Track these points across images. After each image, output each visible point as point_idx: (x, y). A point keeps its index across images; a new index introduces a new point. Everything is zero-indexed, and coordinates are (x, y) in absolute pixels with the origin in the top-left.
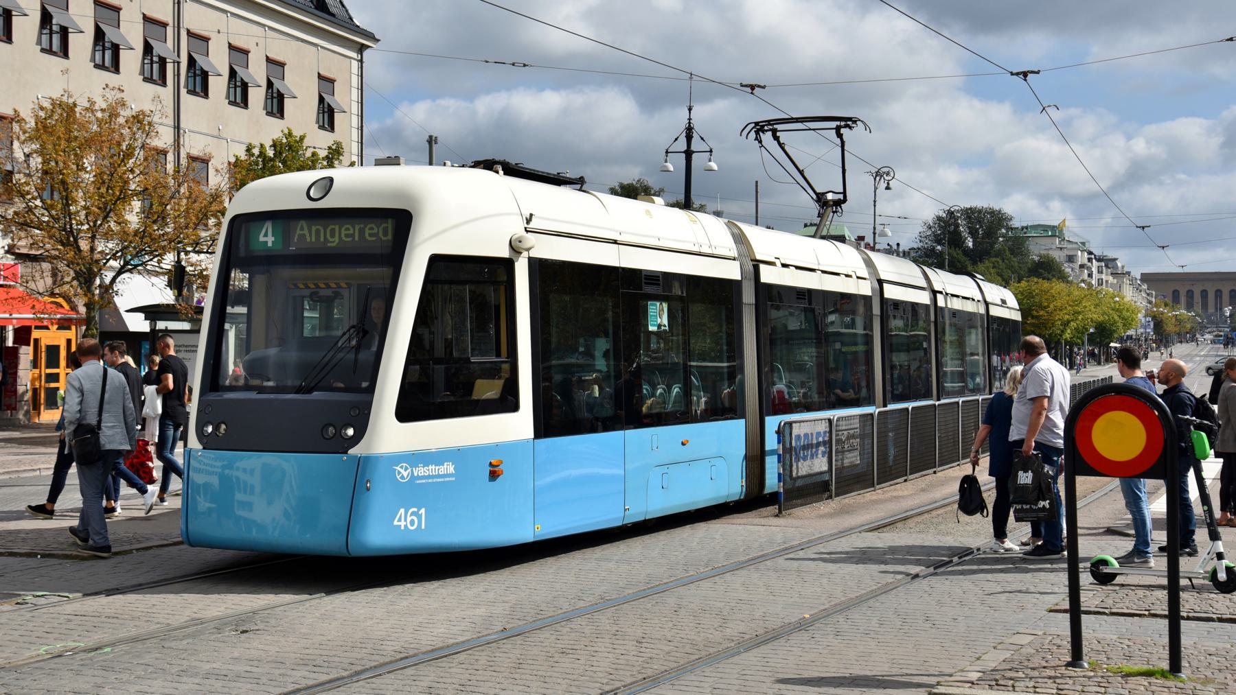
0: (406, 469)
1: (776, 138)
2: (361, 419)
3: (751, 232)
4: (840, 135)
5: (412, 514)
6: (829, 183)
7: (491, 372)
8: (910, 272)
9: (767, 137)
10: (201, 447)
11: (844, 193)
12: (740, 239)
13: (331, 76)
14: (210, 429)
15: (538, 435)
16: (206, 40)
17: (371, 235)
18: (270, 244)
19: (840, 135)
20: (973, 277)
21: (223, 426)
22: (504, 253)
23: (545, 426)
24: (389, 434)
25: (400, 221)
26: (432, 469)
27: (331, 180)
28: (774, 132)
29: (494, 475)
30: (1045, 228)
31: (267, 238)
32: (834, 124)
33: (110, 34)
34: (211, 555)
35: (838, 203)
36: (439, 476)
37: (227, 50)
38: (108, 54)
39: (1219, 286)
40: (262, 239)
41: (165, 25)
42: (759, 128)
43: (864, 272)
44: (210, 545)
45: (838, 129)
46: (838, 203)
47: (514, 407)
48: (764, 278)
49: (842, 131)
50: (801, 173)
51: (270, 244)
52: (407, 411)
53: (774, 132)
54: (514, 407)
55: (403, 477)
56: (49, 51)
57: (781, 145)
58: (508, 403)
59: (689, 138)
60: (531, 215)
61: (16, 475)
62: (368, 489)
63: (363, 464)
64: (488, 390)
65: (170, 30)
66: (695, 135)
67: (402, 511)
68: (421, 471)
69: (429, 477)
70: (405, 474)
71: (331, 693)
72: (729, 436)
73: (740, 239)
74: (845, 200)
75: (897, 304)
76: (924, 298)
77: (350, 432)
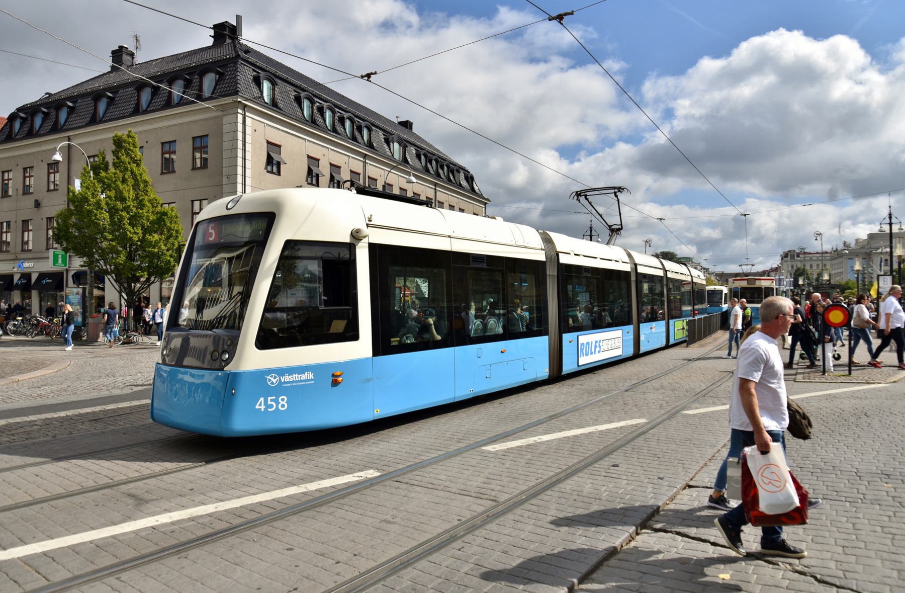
0: (275, 377)
1: (587, 199)
2: (231, 346)
3: (555, 236)
4: (616, 196)
6: (614, 221)
7: (338, 316)
8: (655, 262)
9: (582, 199)
12: (548, 241)
13: (317, 157)
15: (376, 353)
16: (280, 146)
19: (616, 196)
20: (685, 265)
22: (347, 239)
23: (382, 346)
24: (251, 358)
25: (266, 219)
26: (296, 377)
29: (335, 383)
30: (687, 258)
32: (613, 191)
33: (315, 170)
34: (173, 433)
35: (619, 230)
36: (301, 381)
38: (314, 179)
41: (359, 174)
42: (578, 194)
43: (627, 259)
44: (166, 425)
45: (615, 193)
46: (619, 230)
47: (355, 337)
48: (561, 261)
52: (265, 341)
53: (586, 196)
54: (355, 337)
55: (272, 383)
56: (272, 172)
57: (590, 203)
58: (351, 334)
62: (233, 394)
63: (235, 376)
64: (338, 326)
65: (361, 176)
68: (287, 378)
69: (293, 382)
70: (274, 381)
71: (85, 588)
72: (540, 345)
73: (548, 241)
75: (645, 276)
76: (660, 273)
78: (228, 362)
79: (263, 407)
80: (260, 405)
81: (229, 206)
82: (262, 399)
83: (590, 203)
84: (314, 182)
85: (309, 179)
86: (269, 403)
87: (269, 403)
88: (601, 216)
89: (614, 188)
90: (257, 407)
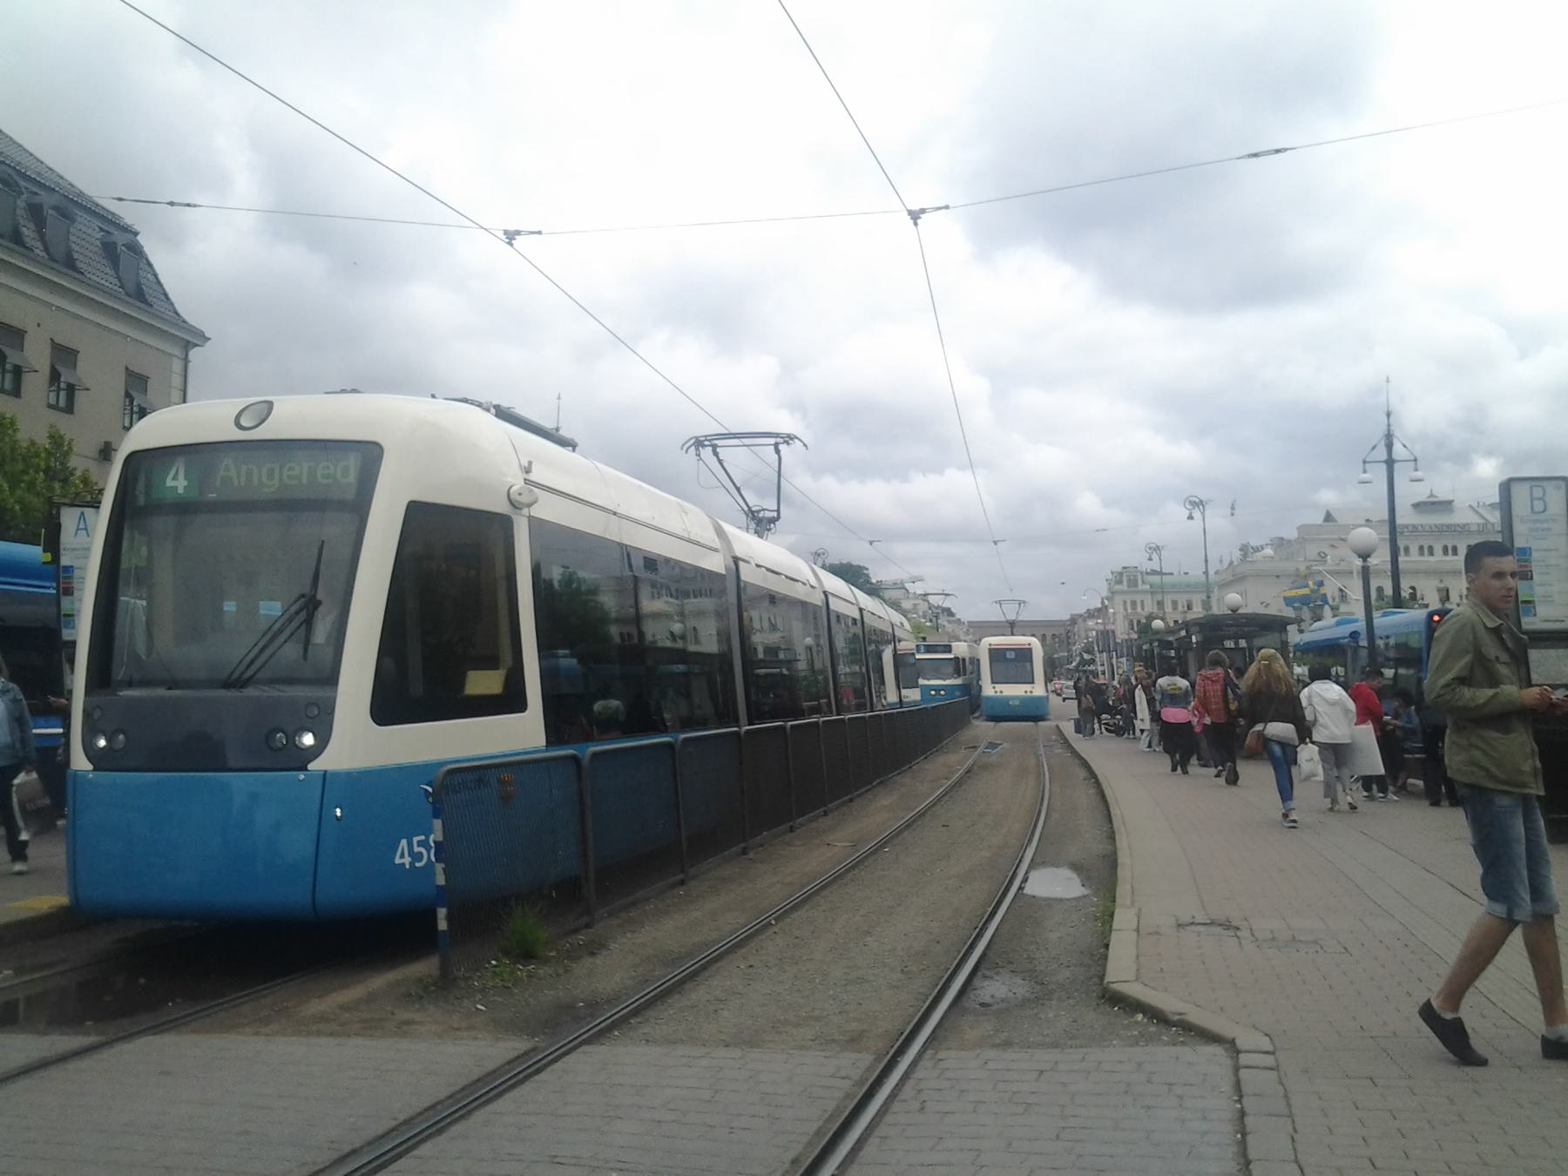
1: (716, 454)
4: (778, 451)
5: (420, 844)
10: (91, 767)
11: (778, 511)
14: (102, 743)
17: (324, 476)
18: (181, 491)
19: (778, 451)
21: (121, 737)
27: (270, 405)
28: (714, 447)
31: (177, 482)
32: (772, 441)
35: (773, 520)
37: (123, 376)
39: (1175, 597)
40: (169, 483)
42: (699, 443)
45: (776, 445)
49: (781, 447)
50: (738, 489)
51: (181, 491)
53: (714, 447)
57: (720, 462)
58: (511, 700)
59: (1389, 446)
60: (530, 463)
61: (1521, 849)
64: (484, 682)
66: (1395, 441)
67: (404, 842)
74: (778, 518)
77: (308, 740)
78: (316, 751)
79: (407, 860)
80: (402, 856)
81: (244, 423)
82: (404, 842)
83: (720, 462)
84: (62, 403)
85: (52, 396)
86: (416, 849)
87: (416, 849)
88: (738, 489)
89: (776, 435)
90: (398, 861)
